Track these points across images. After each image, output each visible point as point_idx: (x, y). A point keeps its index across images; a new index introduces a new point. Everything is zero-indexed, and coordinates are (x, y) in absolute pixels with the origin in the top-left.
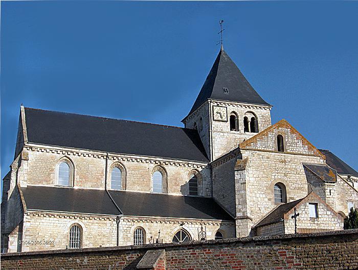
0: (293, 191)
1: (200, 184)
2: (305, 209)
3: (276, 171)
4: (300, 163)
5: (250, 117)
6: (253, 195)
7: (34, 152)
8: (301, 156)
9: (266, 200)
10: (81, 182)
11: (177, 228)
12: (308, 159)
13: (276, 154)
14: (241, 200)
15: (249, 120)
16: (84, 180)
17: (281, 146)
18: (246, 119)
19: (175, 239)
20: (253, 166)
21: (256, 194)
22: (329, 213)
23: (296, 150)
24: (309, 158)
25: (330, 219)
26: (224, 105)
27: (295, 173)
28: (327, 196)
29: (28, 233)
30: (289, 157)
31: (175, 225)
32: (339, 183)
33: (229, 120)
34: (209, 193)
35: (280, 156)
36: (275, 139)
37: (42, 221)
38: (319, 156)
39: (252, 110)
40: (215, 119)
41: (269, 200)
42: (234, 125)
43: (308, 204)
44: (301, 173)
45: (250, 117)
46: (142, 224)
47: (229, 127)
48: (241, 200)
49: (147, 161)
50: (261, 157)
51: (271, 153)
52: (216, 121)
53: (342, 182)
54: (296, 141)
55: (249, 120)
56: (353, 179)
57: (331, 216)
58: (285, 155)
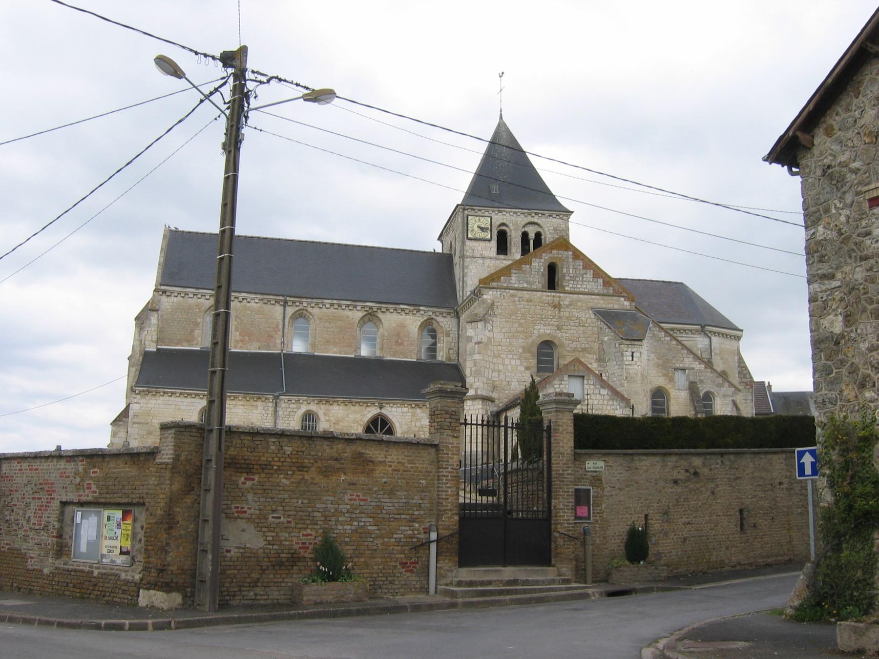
0: (571, 354)
1: (439, 342)
2: (559, 385)
3: (543, 323)
4: (588, 309)
5: (532, 232)
6: (500, 361)
7: (169, 298)
8: (589, 296)
9: (522, 369)
10: (242, 341)
11: (371, 412)
12: (602, 302)
13: (544, 293)
14: (474, 369)
15: (532, 236)
16: (247, 338)
17: (220, 329)
18: (525, 236)
19: (368, 430)
20: (501, 314)
21: (503, 359)
22: (604, 392)
23: (581, 287)
24: (604, 300)
25: (605, 402)
26: (487, 214)
27: (578, 324)
28: (626, 363)
29: (136, 420)
30: (566, 299)
31: (368, 409)
32: (662, 339)
33: (495, 237)
34: (453, 356)
35: (549, 296)
36: (544, 270)
37: (158, 402)
38: (623, 297)
39: (535, 220)
40: (470, 236)
41: (527, 368)
42: (503, 246)
43: (566, 378)
44: (586, 325)
45: (532, 232)
46: (313, 407)
47: (495, 249)
48: (474, 369)
49: (351, 308)
50: (516, 299)
51: (534, 293)
52: (471, 239)
53: (668, 339)
54: (582, 272)
55: (532, 236)
56: (710, 332)
57: (607, 397)
58: (561, 295)
